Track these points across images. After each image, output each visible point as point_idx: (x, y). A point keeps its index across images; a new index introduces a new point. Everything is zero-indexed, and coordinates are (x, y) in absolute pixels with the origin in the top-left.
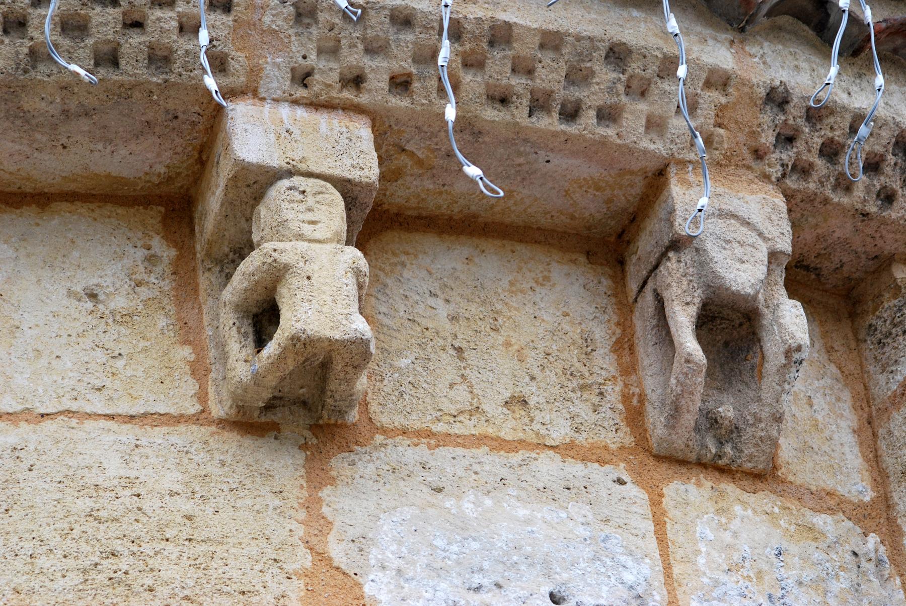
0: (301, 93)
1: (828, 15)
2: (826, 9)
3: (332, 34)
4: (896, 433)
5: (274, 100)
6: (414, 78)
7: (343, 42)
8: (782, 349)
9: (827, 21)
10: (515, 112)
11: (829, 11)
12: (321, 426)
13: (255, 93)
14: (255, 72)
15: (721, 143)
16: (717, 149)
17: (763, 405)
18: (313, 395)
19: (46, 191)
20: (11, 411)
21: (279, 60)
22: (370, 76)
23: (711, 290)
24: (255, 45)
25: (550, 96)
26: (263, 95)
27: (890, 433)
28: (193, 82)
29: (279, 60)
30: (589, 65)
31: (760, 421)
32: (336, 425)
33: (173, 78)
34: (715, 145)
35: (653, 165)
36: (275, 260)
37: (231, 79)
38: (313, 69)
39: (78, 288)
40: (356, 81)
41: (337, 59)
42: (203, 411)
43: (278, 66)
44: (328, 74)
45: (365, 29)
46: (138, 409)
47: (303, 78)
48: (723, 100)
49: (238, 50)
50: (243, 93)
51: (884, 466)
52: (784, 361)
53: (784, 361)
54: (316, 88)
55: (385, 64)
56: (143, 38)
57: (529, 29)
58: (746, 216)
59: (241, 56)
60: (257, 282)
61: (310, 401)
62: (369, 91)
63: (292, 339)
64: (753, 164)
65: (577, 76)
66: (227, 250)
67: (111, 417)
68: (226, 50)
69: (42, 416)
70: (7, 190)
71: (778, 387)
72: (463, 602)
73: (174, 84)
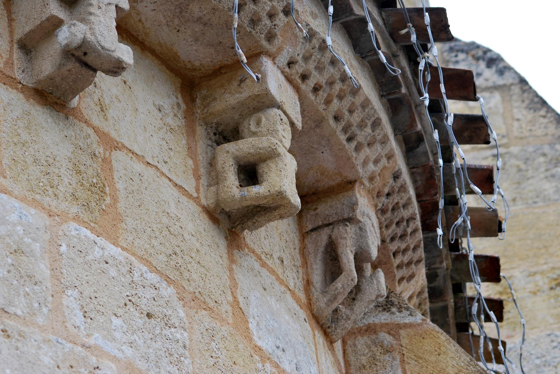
0: (287, 69)
1: (418, 147)
2: (420, 144)
3: (312, 51)
4: (359, 347)
5: (278, 66)
6: (322, 89)
7: (313, 57)
8: (376, 293)
9: (416, 149)
10: (339, 126)
11: (420, 146)
12: (232, 232)
13: (273, 60)
14: (280, 49)
15: (376, 182)
16: (373, 184)
17: (353, 313)
18: (236, 216)
19: (146, 43)
20: (138, 153)
21: (290, 50)
22: (311, 78)
23: (361, 250)
24: (287, 37)
25: (350, 126)
26: (276, 62)
27: (355, 345)
28: (259, 39)
29: (290, 50)
30: (368, 121)
31: (349, 319)
32: (237, 234)
33: (253, 32)
34: (373, 182)
35: (351, 177)
36: (276, 149)
37: (271, 47)
38: (297, 62)
39: (157, 103)
40: (304, 77)
41: (306, 64)
42: (197, 198)
43: (288, 52)
44: (299, 68)
45: (322, 56)
46: (179, 182)
47: (290, 64)
48: (387, 165)
49: (281, 36)
50: (270, 56)
51: (349, 359)
52: (374, 299)
53: (374, 299)
54: (294, 71)
55: (318, 76)
56: (254, 7)
57: (364, 93)
58: (149, 168)
59: (281, 39)
60: (260, 153)
61: (232, 217)
62: (307, 85)
63: (279, 192)
64: (375, 198)
65: (362, 125)
66: (215, 121)
67: (170, 180)
68: (278, 33)
69: (148, 163)
70: (133, 33)
71: (364, 308)
72: (421, 373)
73: (253, 36)
